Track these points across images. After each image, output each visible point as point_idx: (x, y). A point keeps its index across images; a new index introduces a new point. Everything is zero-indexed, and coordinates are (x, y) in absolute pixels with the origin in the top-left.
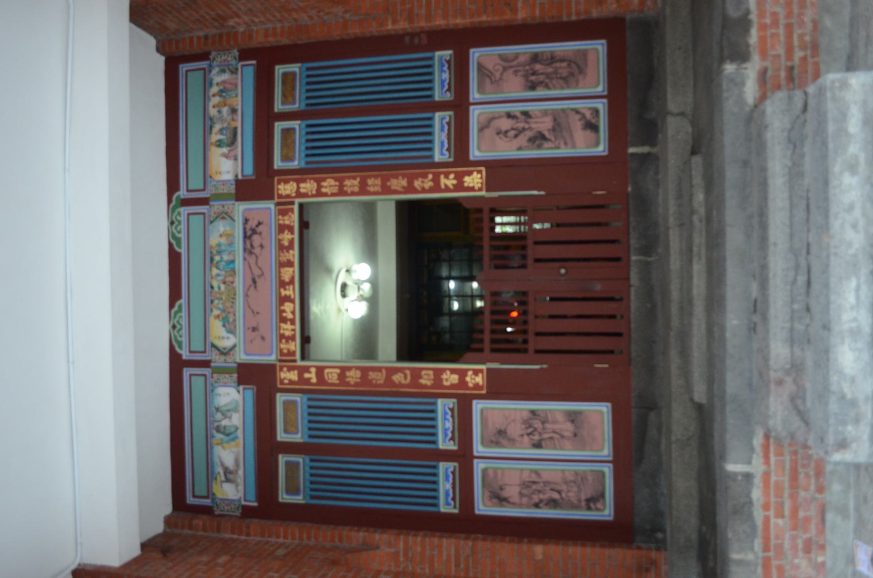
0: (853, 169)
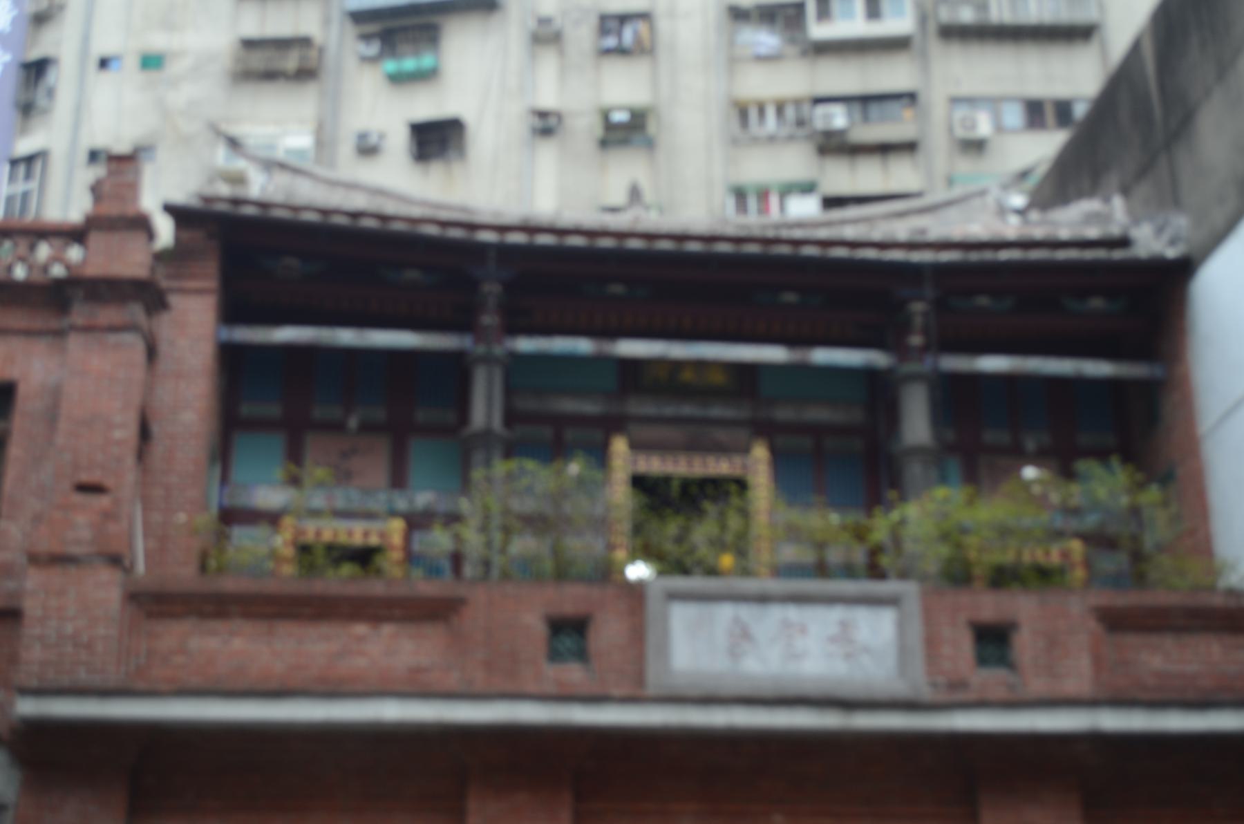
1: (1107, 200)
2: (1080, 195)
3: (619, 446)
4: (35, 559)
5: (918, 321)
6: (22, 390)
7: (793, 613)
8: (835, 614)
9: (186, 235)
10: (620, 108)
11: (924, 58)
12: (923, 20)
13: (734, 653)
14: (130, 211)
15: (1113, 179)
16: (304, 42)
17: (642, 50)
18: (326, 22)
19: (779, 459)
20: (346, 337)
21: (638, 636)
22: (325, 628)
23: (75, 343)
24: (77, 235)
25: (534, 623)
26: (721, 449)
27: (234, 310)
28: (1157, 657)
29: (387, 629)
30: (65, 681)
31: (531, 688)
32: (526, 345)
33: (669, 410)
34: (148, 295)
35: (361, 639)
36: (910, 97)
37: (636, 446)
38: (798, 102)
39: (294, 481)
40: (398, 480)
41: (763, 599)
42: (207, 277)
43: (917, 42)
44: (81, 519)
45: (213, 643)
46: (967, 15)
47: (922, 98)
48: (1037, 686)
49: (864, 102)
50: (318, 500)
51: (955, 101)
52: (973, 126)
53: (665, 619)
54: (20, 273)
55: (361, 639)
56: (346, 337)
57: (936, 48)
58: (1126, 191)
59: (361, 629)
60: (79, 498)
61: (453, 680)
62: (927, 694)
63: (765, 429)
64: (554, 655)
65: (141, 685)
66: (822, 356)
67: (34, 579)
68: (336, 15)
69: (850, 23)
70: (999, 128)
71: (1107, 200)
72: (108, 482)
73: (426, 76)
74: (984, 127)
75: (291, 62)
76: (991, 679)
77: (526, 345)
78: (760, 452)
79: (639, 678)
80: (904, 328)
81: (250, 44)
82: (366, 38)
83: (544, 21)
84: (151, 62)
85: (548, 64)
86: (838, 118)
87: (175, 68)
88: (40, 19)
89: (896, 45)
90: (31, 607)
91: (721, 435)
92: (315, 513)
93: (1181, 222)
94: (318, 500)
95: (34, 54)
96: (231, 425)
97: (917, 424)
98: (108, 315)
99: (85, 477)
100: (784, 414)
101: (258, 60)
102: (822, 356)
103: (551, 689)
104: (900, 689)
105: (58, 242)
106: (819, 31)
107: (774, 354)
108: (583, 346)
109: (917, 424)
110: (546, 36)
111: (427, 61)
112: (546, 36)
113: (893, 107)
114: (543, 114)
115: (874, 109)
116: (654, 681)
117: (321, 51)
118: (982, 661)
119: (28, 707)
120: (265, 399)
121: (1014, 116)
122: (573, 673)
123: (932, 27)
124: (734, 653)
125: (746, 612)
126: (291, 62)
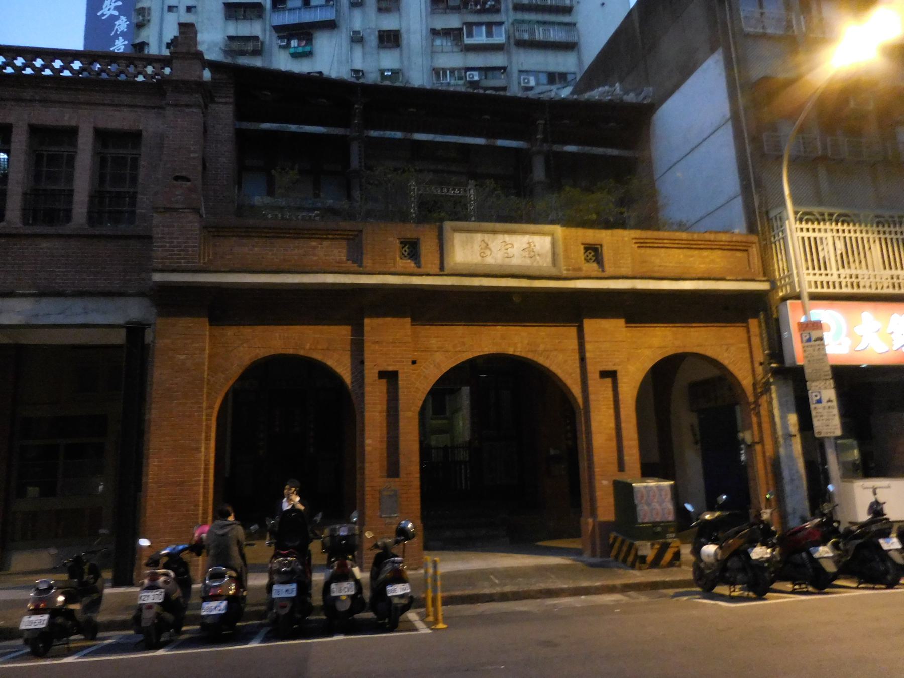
1: (612, 85)
4: (156, 209)
5: (541, 128)
6: (144, 133)
9: (217, 77)
10: (388, 70)
11: (509, 53)
12: (508, 38)
14: (193, 50)
16: (256, 38)
18: (264, 30)
20: (293, 127)
22: (297, 242)
23: (169, 112)
26: (457, 185)
27: (240, 115)
29: (326, 243)
31: (393, 270)
32: (373, 133)
33: (440, 167)
34: (207, 92)
35: (315, 248)
36: (504, 69)
38: (459, 69)
39: (271, 193)
40: (317, 196)
43: (506, 47)
46: (526, 36)
49: (486, 71)
50: (282, 202)
51: (521, 72)
52: (528, 82)
54: (140, 78)
55: (315, 248)
57: (514, 49)
58: (621, 81)
59: (314, 243)
63: (473, 176)
65: (212, 268)
66: (500, 142)
67: (157, 219)
68: (268, 27)
69: (480, 37)
70: (538, 84)
72: (191, 177)
73: (309, 54)
74: (532, 83)
75: (250, 47)
77: (373, 133)
79: (442, 267)
81: (231, 38)
82: (280, 37)
83: (355, 32)
85: (358, 52)
88: (140, 26)
92: (281, 209)
93: (650, 90)
94: (282, 202)
95: (137, 41)
96: (242, 170)
97: (539, 173)
98: (185, 99)
101: (235, 46)
102: (500, 142)
103: (402, 270)
104: (554, 272)
105: (157, 65)
106: (467, 41)
108: (399, 135)
109: (539, 173)
110: (357, 39)
111: (308, 49)
112: (357, 39)
113: (497, 73)
115: (490, 74)
116: (449, 265)
117: (262, 43)
118: (587, 260)
119: (157, 277)
120: (257, 154)
121: (544, 79)
123: (512, 41)
125: (486, 236)
126: (250, 47)
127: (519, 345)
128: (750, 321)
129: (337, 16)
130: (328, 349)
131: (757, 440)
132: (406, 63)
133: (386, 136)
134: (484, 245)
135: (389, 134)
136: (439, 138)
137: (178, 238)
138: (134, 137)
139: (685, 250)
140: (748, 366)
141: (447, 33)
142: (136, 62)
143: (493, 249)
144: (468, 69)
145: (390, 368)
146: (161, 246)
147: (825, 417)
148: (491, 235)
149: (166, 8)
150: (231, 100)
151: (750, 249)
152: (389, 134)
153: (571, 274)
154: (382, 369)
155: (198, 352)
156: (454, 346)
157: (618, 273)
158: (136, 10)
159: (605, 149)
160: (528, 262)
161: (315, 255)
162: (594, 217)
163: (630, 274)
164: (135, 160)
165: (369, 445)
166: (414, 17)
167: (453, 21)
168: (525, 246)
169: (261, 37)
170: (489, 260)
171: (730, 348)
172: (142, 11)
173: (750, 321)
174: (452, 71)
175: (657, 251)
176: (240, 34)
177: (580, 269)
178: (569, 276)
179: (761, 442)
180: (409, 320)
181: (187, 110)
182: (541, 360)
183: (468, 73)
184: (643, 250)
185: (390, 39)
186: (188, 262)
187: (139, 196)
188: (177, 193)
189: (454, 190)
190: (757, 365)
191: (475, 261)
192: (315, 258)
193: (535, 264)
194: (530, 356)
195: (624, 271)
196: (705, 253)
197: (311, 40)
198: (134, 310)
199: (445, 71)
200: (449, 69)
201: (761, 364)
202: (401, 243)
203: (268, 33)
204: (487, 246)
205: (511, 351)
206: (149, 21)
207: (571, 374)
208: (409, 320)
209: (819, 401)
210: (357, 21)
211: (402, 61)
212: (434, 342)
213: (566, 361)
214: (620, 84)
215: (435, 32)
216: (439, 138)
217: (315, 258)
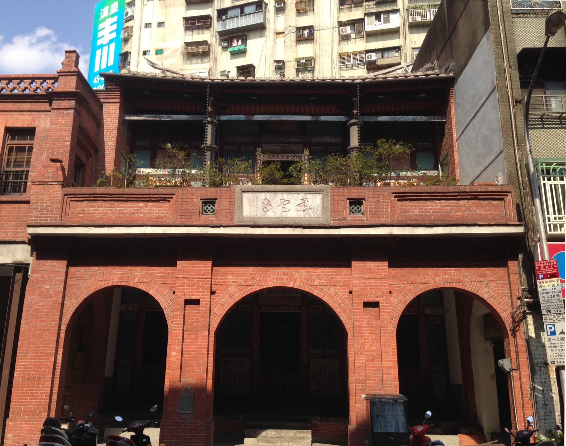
0: (295, 434)
2: (427, 62)
3: (259, 150)
7: (285, 196)
8: (301, 196)
10: (303, 58)
13: (264, 210)
15: (434, 55)
16: (205, 43)
17: (310, 39)
19: (311, 153)
20: (164, 118)
21: (231, 204)
22: (129, 204)
24: (55, 79)
25: (197, 202)
26: (293, 152)
28: (418, 209)
29: (150, 204)
30: (43, 222)
32: (224, 118)
35: (141, 207)
37: (263, 152)
38: (361, 53)
41: (276, 192)
42: (116, 97)
43: (401, 30)
44: (196, 200)
45: (92, 210)
46: (419, 19)
47: (403, 49)
48: (371, 221)
53: (242, 199)
56: (164, 118)
59: (141, 204)
60: (51, 163)
61: (171, 221)
62: (332, 223)
64: (204, 212)
71: (432, 63)
76: (353, 218)
77: (224, 118)
78: (306, 152)
79: (232, 219)
80: (353, 108)
81: (188, 44)
84: (159, 52)
86: (374, 57)
87: (166, 54)
88: (126, 40)
89: (395, 32)
90: (33, 199)
91: (293, 147)
99: (55, 158)
100: (315, 140)
103: (200, 223)
104: (323, 222)
107: (307, 118)
109: (354, 140)
111: (243, 47)
114: (277, 62)
115: (386, 55)
117: (210, 45)
119: (31, 230)
122: (210, 218)
124: (264, 210)
125: (269, 196)
127: (298, 280)
128: (510, 263)
129: (265, 19)
130: (151, 282)
131: (515, 367)
132: (318, 52)
133: (233, 119)
134: (266, 202)
135: (234, 117)
136: (274, 118)
137: (46, 203)
138: (30, 132)
139: (443, 201)
140: (507, 299)
141: (352, 23)
142: (36, 81)
143: (273, 205)
144: (368, 51)
145: (194, 297)
146: (35, 209)
147: (558, 348)
148: (272, 195)
149: (143, 26)
150: (118, 100)
151: (506, 198)
152: (234, 117)
153: (337, 223)
154: (188, 298)
155: (58, 283)
156: (246, 281)
157: (379, 223)
158: (124, 29)
159: (415, 117)
160: (301, 214)
161: (141, 213)
162: (192, 183)
163: (389, 222)
164: (31, 149)
165: (174, 356)
166: (327, 12)
167: (358, 14)
168: (300, 202)
169: (209, 42)
170: (270, 214)
171: (493, 286)
172: (127, 29)
173: (510, 263)
174: (355, 54)
175: (416, 203)
176: (194, 40)
177: (345, 219)
178: (334, 225)
179: (518, 369)
180: (386, 263)
181: (66, 112)
182: (316, 293)
183: (367, 54)
184: (403, 203)
185: (305, 35)
186: (52, 220)
187: (30, 174)
188: (49, 171)
189: (292, 156)
190: (515, 299)
191: (259, 215)
192: (141, 215)
193: (307, 216)
194: (307, 289)
195: (383, 221)
196: (461, 203)
197: (246, 40)
198: (22, 254)
199: (349, 55)
200: (353, 53)
201: (519, 298)
202: (204, 203)
203: (214, 38)
204: (269, 204)
205: (291, 285)
206: (132, 36)
207: (340, 304)
208: (386, 263)
209: (553, 333)
210: (276, 22)
211: (315, 51)
212: (230, 278)
213: (337, 293)
214: (437, 60)
215: (341, 24)
216: (274, 118)
217: (141, 215)
